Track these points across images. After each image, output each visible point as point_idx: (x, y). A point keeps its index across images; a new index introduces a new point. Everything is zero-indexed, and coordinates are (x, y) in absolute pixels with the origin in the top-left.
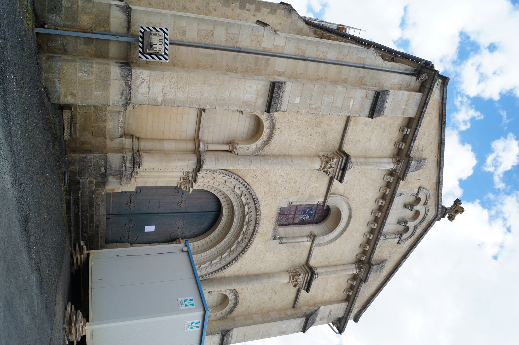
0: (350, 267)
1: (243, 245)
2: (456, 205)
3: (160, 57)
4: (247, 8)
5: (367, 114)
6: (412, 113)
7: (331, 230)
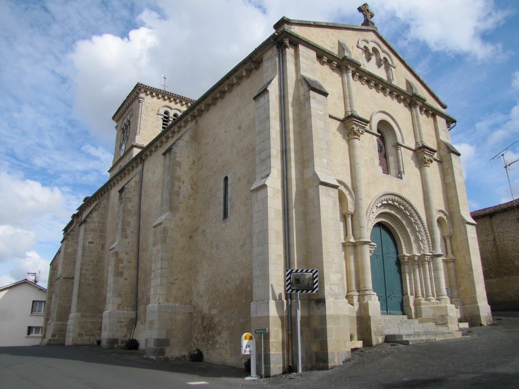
0: (415, 112)
1: (407, 205)
2: (363, 10)
3: (315, 276)
4: (178, 190)
5: (325, 97)
6: (313, 54)
7: (392, 128)
